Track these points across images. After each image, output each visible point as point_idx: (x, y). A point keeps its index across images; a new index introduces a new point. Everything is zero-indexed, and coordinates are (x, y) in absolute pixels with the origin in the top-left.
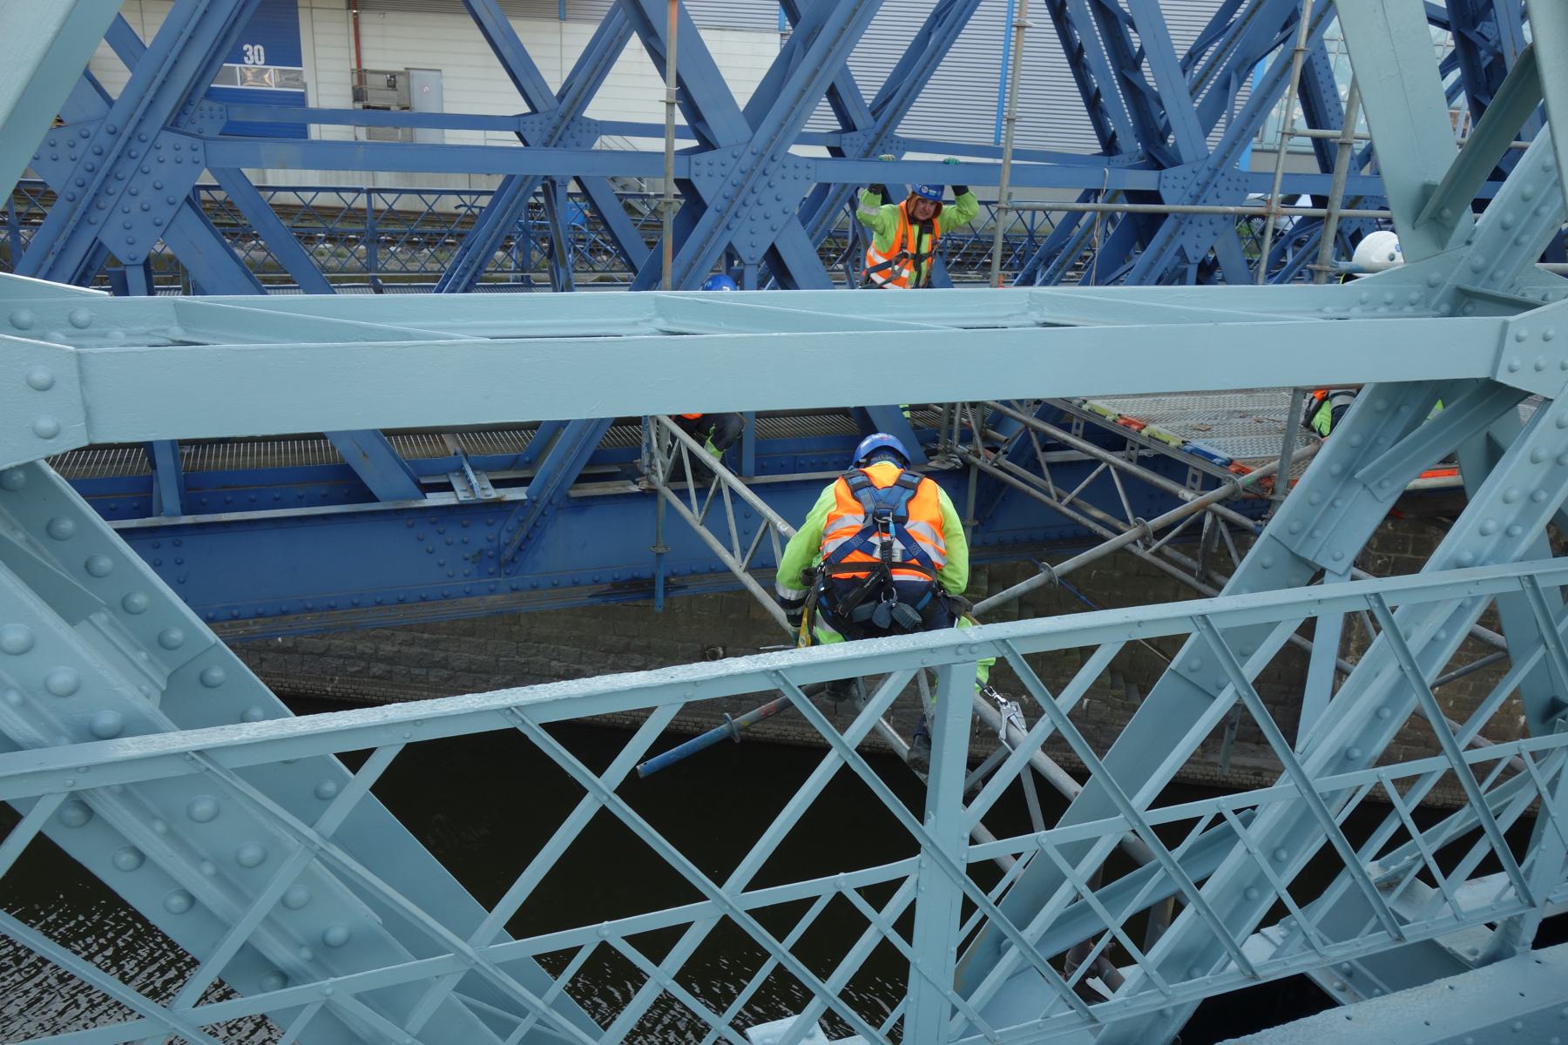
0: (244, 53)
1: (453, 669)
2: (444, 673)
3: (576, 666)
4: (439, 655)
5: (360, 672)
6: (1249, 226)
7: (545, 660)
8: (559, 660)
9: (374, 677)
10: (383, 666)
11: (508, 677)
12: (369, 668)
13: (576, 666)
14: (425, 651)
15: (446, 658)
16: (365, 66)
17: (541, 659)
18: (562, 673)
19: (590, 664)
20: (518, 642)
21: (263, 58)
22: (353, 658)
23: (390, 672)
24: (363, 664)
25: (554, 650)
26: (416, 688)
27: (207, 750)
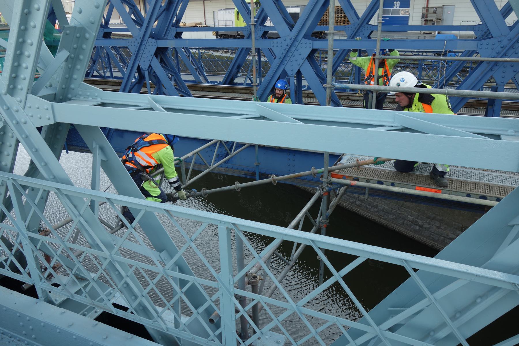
0: (394, 5)
1: (378, 209)
2: (376, 210)
3: (416, 220)
4: (375, 204)
5: (353, 202)
6: (378, 69)
7: (407, 214)
8: (411, 216)
9: (357, 205)
10: (359, 202)
11: (394, 217)
12: (356, 202)
13: (416, 220)
14: (372, 201)
15: (377, 205)
16: (430, 6)
17: (405, 214)
18: (411, 220)
19: (421, 220)
20: (399, 206)
21: (399, 6)
22: (352, 197)
23: (361, 205)
24: (354, 200)
25: (410, 212)
26: (367, 212)
27: (408, 261)
